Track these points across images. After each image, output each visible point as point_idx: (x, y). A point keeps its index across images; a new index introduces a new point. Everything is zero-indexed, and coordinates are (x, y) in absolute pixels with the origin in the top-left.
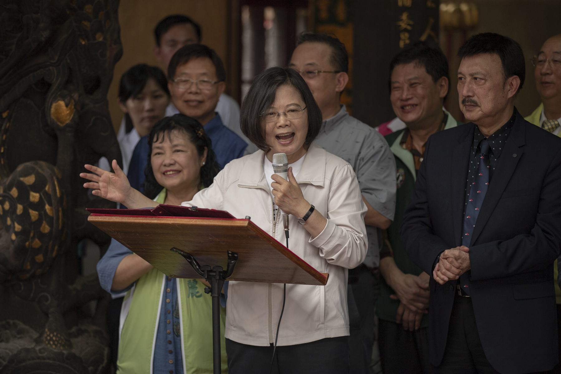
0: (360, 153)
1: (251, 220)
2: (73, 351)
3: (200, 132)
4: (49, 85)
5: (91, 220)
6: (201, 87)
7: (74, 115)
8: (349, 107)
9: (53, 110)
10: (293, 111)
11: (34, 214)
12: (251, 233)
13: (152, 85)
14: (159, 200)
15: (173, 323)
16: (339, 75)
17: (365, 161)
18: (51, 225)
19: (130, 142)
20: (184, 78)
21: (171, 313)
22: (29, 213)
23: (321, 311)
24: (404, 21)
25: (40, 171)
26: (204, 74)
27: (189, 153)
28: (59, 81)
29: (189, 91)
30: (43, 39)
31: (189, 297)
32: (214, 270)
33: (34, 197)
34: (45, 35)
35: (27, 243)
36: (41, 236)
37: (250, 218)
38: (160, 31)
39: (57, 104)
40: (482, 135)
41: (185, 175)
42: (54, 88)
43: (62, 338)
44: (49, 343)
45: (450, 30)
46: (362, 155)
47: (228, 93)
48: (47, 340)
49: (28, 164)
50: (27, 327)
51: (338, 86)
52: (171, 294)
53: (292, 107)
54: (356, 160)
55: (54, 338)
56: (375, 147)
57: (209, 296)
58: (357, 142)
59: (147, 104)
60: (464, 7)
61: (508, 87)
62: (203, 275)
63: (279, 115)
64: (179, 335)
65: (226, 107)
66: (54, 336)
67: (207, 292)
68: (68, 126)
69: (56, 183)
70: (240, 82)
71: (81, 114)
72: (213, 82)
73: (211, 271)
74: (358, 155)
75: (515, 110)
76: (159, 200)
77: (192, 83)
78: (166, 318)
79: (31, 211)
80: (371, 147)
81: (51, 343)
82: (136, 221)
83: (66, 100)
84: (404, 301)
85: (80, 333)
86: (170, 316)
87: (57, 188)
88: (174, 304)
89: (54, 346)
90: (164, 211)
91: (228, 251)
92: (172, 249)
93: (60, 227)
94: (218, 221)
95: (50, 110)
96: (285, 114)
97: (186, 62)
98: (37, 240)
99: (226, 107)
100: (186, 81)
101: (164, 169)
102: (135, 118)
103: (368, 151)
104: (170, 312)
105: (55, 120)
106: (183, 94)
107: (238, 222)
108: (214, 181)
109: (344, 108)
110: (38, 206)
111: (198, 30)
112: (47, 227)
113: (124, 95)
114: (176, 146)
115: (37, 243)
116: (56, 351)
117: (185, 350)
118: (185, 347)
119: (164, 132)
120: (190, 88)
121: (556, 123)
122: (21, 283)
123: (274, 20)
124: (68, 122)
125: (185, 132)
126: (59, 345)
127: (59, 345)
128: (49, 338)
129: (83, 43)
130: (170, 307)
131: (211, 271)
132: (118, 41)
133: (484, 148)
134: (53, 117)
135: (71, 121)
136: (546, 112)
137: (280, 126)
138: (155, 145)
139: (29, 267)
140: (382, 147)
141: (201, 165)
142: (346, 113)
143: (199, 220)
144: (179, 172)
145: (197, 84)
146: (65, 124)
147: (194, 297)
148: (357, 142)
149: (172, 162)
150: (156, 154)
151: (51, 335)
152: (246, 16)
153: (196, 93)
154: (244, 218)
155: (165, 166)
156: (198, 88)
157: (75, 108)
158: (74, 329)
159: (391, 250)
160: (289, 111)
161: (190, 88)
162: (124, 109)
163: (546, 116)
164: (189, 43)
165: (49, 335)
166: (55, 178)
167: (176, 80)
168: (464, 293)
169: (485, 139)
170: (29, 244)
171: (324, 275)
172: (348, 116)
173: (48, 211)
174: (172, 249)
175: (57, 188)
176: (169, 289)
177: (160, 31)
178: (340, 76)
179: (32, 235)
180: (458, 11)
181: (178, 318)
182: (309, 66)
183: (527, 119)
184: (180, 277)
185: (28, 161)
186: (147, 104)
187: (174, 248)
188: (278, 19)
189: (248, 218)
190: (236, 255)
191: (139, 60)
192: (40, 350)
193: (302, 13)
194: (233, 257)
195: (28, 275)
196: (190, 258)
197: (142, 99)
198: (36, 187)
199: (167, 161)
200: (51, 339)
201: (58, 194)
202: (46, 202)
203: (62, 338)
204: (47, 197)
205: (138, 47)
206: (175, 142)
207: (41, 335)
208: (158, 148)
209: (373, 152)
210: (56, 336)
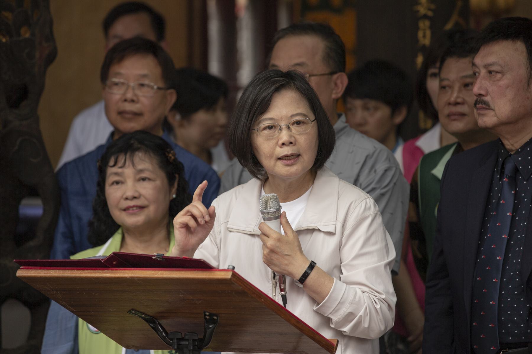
1: (236, 270)
3: (170, 155)
5: (21, 275)
10: (298, 123)
12: (236, 288)
16: (335, 76)
26: (144, 76)
27: (158, 183)
32: (187, 337)
37: (234, 268)
40: (507, 151)
41: (151, 211)
51: (334, 91)
53: (298, 118)
56: (378, 171)
58: (332, 162)
63: (281, 129)
82: (82, 275)
90: (119, 260)
91: (204, 313)
92: (129, 312)
94: (192, 272)
96: (289, 128)
101: (125, 204)
107: (219, 273)
114: (141, 171)
119: (126, 154)
125: (152, 154)
131: (183, 339)
133: (509, 168)
137: (283, 144)
138: (110, 170)
141: (171, 198)
144: (142, 208)
149: (136, 195)
150: (113, 183)
153: (133, 101)
154: (226, 268)
155: (127, 199)
156: (136, 95)
160: (293, 124)
171: (332, 342)
174: (129, 312)
178: (338, 78)
189: (231, 267)
190: (215, 317)
196: (154, 323)
199: (129, 194)
206: (140, 167)
208: (116, 174)
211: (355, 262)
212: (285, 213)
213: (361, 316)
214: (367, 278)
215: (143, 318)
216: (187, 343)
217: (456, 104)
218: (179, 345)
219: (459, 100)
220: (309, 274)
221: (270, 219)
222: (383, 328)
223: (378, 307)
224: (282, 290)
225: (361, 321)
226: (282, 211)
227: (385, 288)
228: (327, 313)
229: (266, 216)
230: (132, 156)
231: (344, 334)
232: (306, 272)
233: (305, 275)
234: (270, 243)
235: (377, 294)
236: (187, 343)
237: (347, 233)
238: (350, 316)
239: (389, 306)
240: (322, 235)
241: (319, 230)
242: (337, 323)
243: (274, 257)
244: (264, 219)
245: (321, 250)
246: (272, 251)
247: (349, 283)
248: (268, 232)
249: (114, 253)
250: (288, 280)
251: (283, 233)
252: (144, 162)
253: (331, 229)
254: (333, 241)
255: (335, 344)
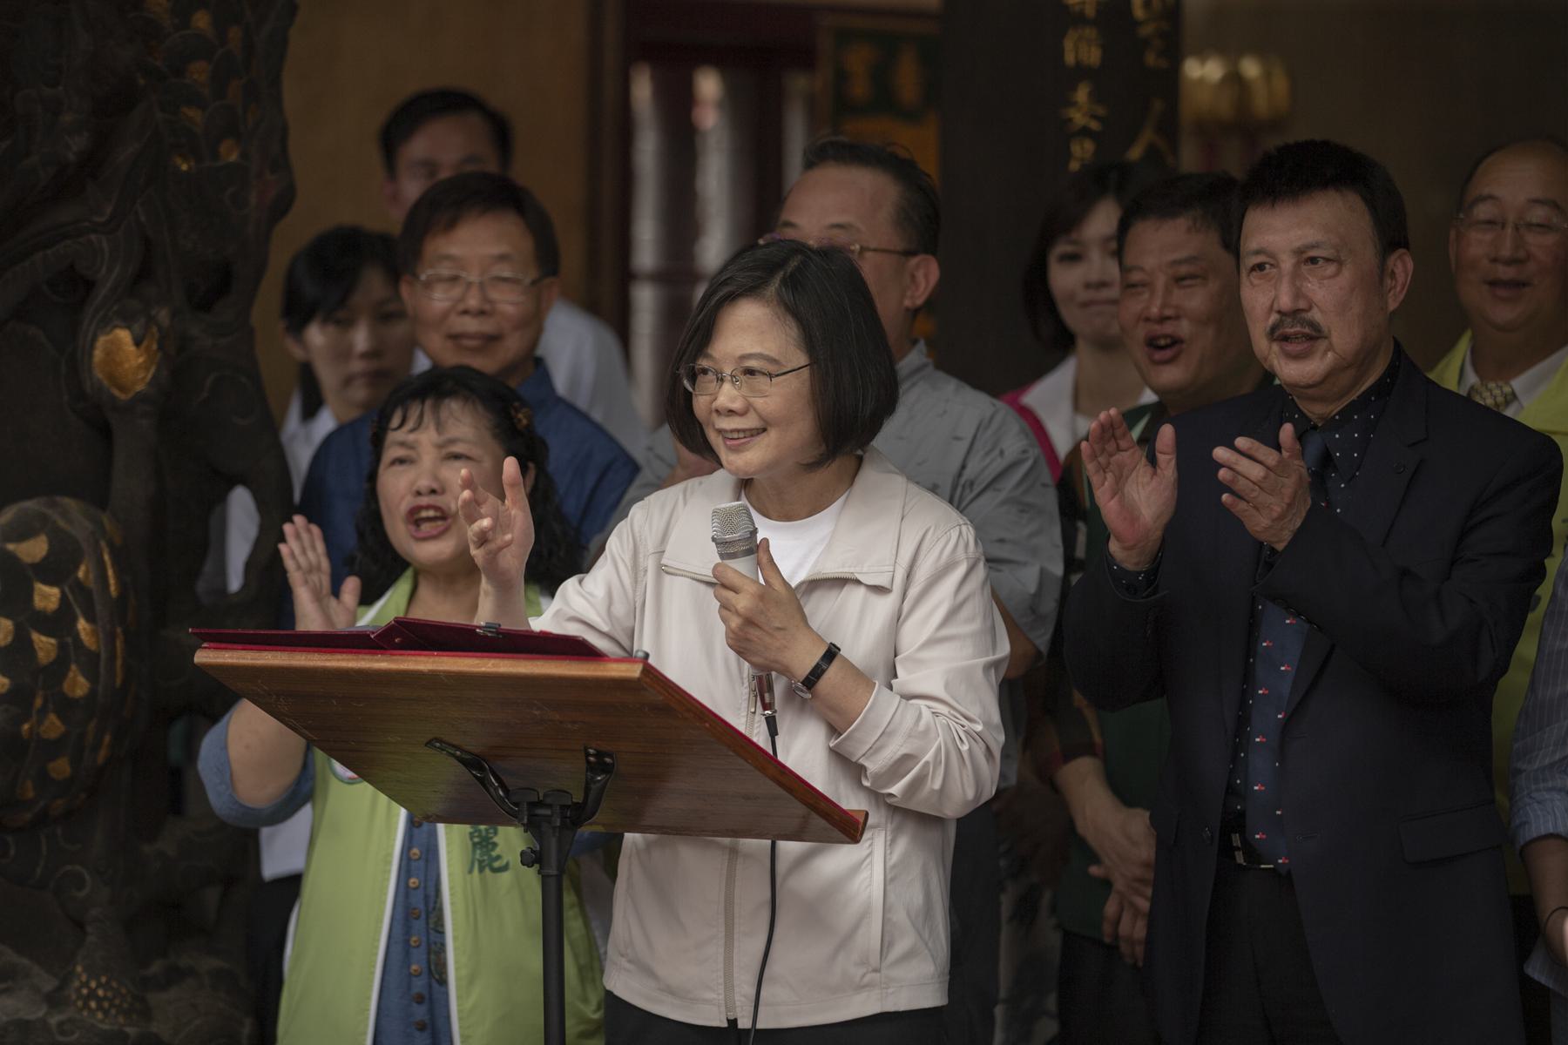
0: (963, 467)
1: (651, 661)
2: (154, 1028)
3: (520, 416)
4: (90, 285)
5: (204, 660)
6: (494, 295)
7: (158, 370)
8: (931, 345)
9: (98, 354)
11: (44, 645)
13: (373, 284)
14: (389, 607)
15: (429, 945)
16: (914, 261)
17: (977, 490)
18: (93, 677)
19: (304, 440)
20: (445, 270)
21: (423, 916)
22: (31, 642)
23: (875, 913)
24: (1082, 107)
25: (61, 523)
26: (502, 258)
28: (117, 270)
29: (461, 307)
30: (71, 157)
31: (471, 871)
32: (548, 801)
33: (45, 596)
34: (77, 144)
35: (26, 727)
36: (66, 706)
37: (647, 655)
38: (392, 138)
39: (110, 337)
42: (102, 292)
43: (124, 991)
44: (86, 1006)
45: (1211, 132)
46: (968, 474)
47: (590, 306)
48: (80, 996)
49: (30, 505)
50: (25, 961)
52: (422, 863)
54: (954, 488)
55: (100, 992)
57: (531, 876)
58: (957, 439)
59: (361, 338)
60: (1251, 68)
61: (1388, 281)
62: (515, 815)
64: (443, 982)
65: (570, 345)
66: (99, 985)
67: (529, 859)
68: (141, 398)
69: (106, 557)
70: (626, 277)
71: (178, 366)
72: (528, 281)
73: (540, 804)
74: (960, 475)
75: (1397, 345)
76: (389, 607)
77: (469, 285)
78: (408, 932)
79: (35, 636)
80: (997, 452)
81: (93, 1004)
82: (328, 664)
83: (136, 327)
84: (1119, 885)
85: (174, 976)
86: (419, 925)
87: (110, 572)
88: (432, 892)
89: (100, 1015)
90: (409, 635)
91: (586, 749)
92: (429, 743)
93: (118, 682)
94: (558, 663)
95: (91, 356)
97: (451, 225)
98: (52, 717)
99: (570, 345)
100: (454, 279)
102: (328, 377)
103: (988, 460)
104: (418, 913)
105: (106, 383)
106: (445, 315)
108: (617, 543)
109: (922, 345)
110: (58, 623)
111: (501, 133)
112: (81, 679)
113: (298, 314)
114: (452, 441)
115: (53, 726)
116: (106, 1027)
117: (460, 1019)
118: (460, 1011)
119: (423, 403)
120: (462, 299)
121: (1507, 389)
122: (10, 839)
123: (720, 105)
124: (140, 387)
125: (480, 408)
126: (113, 1011)
127: (113, 1011)
128: (85, 991)
129: (184, 167)
130: (417, 901)
131: (540, 804)
132: (281, 163)
134: (99, 374)
135: (150, 384)
136: (1477, 358)
138: (393, 436)
139: (31, 794)
140: (1024, 452)
142: (925, 360)
143: (506, 662)
145: (482, 286)
146: (130, 395)
147: (487, 870)
148: (957, 439)
151: (93, 984)
152: (643, 90)
153: (482, 313)
156: (485, 299)
157: (161, 348)
158: (156, 967)
159: (1097, 738)
161: (462, 299)
162: (298, 353)
163: (1477, 371)
164: (470, 168)
165: (86, 985)
166: (103, 544)
167: (423, 277)
168: (1253, 854)
169: (1315, 427)
170: (31, 729)
172: (931, 368)
173: (83, 636)
174: (429, 743)
175: (110, 572)
176: (415, 850)
177: (392, 138)
178: (918, 266)
179: (38, 702)
180: (1234, 79)
181: (442, 933)
182: (836, 231)
183: (1432, 376)
184: (449, 819)
185: (29, 497)
186: (361, 338)
187: (437, 740)
188: (733, 101)
190: (608, 760)
191: (346, 215)
192: (61, 1024)
193: (799, 84)
194: (600, 765)
195: (28, 816)
196: (481, 769)
197: (346, 324)
198: (50, 570)
200: (92, 994)
201: (113, 588)
202: (78, 611)
203: (124, 991)
204: (80, 598)
205: (339, 179)
207: (65, 982)
208: (402, 444)
209: (999, 465)
210: (106, 986)
211: (925, 654)
212: (766, 541)
213: (927, 763)
214: (947, 686)
215: (457, 758)
216: (548, 812)
217: (1163, 319)
218: (531, 816)
219: (1168, 312)
220: (823, 671)
221: (733, 556)
222: (970, 794)
223: (965, 748)
224: (765, 707)
225: (926, 776)
226: (759, 537)
227: (982, 712)
228: (858, 753)
229: (727, 549)
230: (436, 408)
231: (889, 801)
232: (817, 666)
233: (812, 680)
234: (742, 602)
235: (965, 722)
236: (548, 812)
237: (913, 591)
238: (906, 760)
239: (988, 748)
240: (862, 590)
241: (858, 582)
242: (877, 777)
243: (754, 633)
244: (722, 556)
245: (855, 625)
246: (749, 622)
247: (909, 697)
248: (736, 581)
249: (397, 620)
250: (779, 687)
251: (762, 581)
252: (463, 423)
253: (882, 581)
254: (884, 607)
255: (862, 820)
